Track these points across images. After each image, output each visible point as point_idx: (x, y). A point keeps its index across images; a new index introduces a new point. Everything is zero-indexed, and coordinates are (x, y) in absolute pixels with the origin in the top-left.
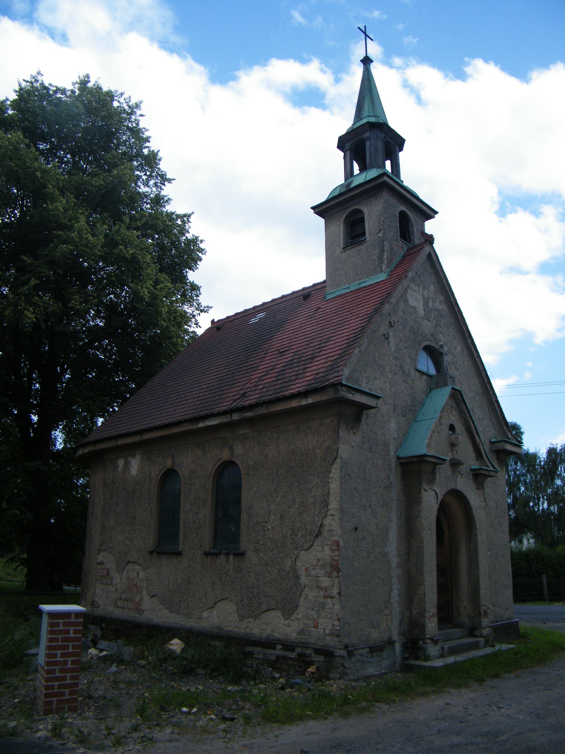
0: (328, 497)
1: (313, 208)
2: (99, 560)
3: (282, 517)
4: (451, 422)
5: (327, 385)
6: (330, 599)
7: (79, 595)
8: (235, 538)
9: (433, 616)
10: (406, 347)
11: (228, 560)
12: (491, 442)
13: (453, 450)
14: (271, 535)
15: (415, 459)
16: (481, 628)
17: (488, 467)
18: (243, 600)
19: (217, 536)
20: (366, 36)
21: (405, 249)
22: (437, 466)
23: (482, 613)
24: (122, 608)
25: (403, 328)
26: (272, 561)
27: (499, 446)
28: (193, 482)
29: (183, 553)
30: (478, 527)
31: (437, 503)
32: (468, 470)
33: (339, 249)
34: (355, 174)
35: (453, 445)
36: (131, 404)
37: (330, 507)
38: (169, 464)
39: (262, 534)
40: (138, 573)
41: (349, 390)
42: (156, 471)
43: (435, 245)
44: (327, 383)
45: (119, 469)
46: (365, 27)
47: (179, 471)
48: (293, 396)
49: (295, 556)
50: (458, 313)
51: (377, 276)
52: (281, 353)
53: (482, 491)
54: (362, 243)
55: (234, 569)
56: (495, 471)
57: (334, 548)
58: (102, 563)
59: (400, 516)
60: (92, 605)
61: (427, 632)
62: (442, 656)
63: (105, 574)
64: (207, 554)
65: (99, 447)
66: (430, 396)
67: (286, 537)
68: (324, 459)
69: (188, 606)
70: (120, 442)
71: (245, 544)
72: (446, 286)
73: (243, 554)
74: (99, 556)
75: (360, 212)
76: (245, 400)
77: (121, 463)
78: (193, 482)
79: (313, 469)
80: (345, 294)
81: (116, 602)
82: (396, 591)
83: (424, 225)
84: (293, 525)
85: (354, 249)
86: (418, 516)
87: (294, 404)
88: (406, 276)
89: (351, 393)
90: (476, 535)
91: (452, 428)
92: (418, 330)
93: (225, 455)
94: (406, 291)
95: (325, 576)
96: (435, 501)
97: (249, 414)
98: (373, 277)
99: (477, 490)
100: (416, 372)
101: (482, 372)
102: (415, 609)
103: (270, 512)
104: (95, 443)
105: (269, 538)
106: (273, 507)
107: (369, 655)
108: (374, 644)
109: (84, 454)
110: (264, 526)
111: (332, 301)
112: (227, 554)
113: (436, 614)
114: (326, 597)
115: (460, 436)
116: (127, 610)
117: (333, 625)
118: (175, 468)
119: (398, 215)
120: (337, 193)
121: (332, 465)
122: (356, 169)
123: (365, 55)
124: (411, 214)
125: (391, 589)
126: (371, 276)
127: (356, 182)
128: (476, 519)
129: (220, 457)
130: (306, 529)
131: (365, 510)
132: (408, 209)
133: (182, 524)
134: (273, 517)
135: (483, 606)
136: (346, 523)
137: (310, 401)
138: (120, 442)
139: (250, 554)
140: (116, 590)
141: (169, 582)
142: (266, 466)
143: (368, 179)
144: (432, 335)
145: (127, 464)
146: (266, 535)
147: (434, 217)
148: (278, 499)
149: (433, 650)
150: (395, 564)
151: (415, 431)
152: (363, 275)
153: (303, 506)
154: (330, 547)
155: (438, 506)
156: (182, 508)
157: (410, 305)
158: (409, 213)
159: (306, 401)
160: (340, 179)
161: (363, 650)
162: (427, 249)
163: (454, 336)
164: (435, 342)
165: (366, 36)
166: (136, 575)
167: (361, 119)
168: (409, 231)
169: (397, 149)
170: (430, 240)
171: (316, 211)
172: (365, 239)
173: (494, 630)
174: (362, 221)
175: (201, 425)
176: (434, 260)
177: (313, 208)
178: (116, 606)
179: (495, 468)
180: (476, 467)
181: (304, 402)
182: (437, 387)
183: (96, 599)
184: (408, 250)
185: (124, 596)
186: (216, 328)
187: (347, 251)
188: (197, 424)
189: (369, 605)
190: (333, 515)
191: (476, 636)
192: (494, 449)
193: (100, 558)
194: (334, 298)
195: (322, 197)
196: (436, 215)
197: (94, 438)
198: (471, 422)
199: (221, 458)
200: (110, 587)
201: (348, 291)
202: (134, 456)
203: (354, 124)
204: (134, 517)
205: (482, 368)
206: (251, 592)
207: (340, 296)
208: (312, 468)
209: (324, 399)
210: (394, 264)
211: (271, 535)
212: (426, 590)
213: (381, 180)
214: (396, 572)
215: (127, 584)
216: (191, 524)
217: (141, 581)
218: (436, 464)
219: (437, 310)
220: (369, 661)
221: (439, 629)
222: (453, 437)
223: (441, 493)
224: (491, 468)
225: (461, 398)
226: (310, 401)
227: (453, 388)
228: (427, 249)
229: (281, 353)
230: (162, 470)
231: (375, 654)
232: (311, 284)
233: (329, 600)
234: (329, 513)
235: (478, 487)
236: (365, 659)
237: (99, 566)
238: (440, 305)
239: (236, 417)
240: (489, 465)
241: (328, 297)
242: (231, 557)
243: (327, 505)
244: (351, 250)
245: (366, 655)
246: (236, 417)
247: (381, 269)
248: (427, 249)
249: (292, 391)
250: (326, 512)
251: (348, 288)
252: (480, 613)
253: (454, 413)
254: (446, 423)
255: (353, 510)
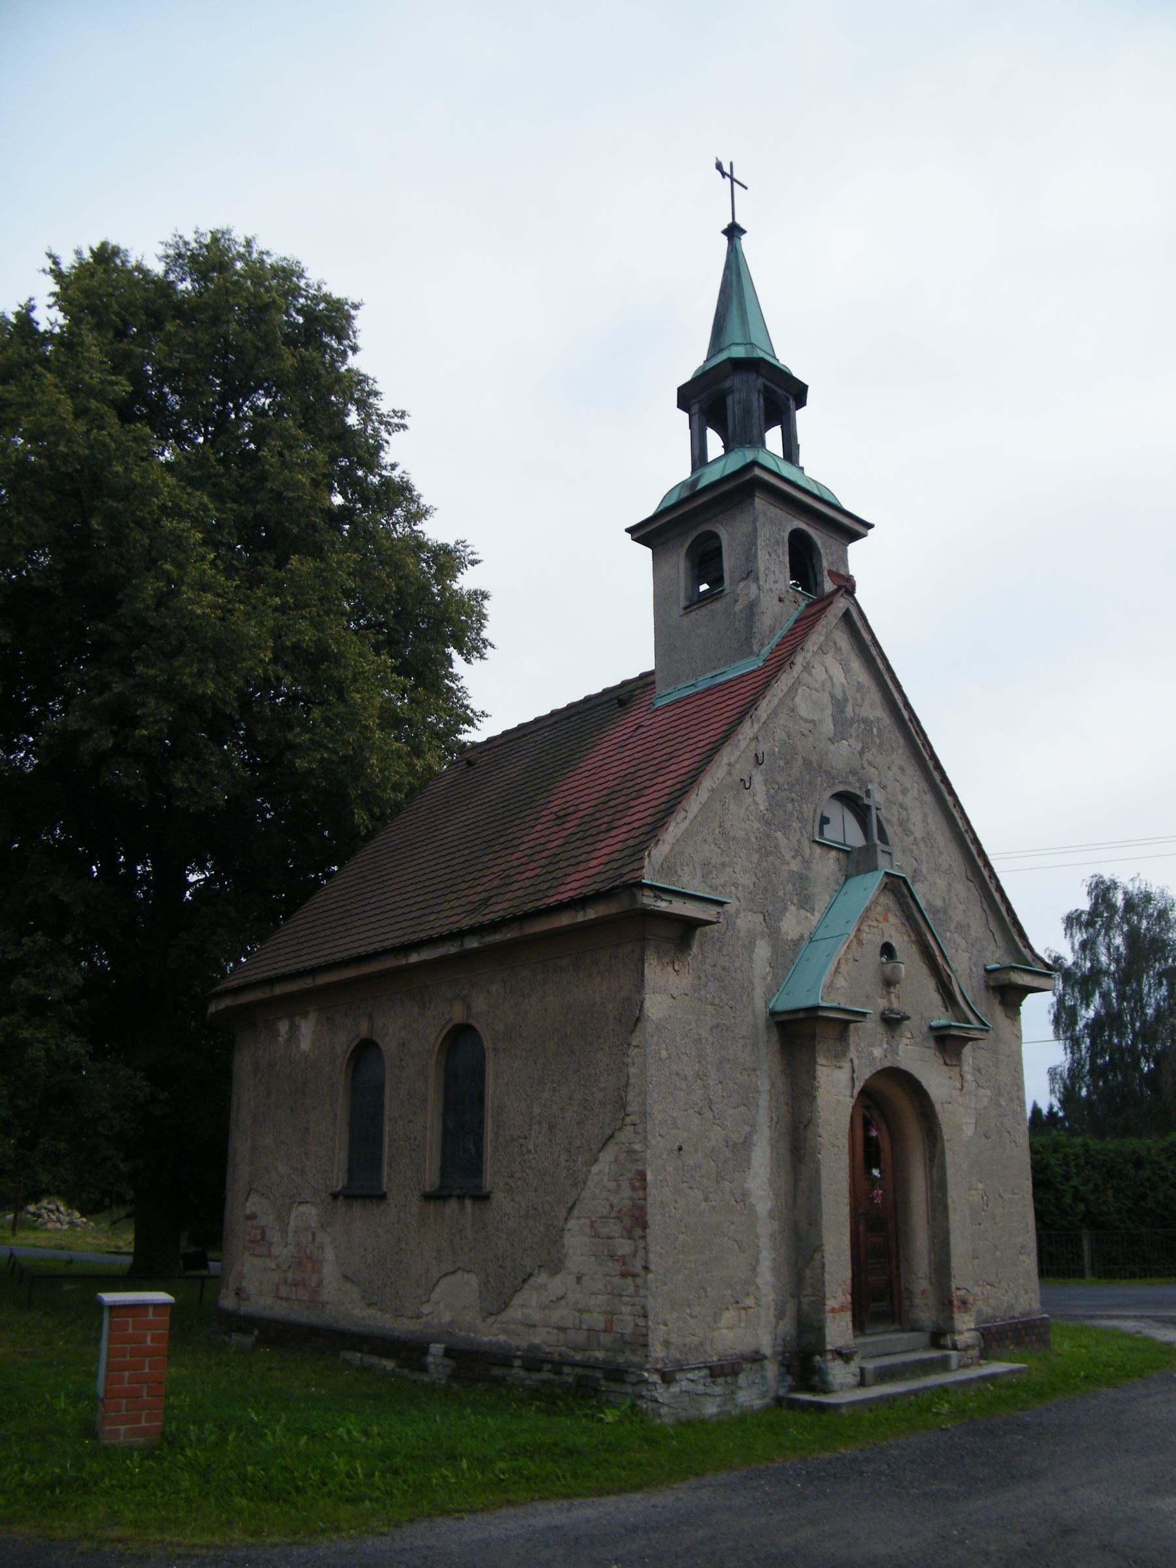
0: (626, 1092)
1: (628, 530)
2: (248, 1211)
3: (551, 1127)
4: (886, 940)
5: (617, 887)
6: (630, 1278)
7: (217, 1277)
8: (475, 1168)
9: (842, 1309)
10: (792, 800)
11: (463, 1208)
12: (986, 970)
13: (889, 993)
14: (533, 1162)
15: (801, 1015)
16: (953, 1333)
17: (969, 1022)
18: (489, 1282)
19: (448, 1165)
20: (733, 180)
21: (803, 604)
22: (852, 1026)
23: (956, 1302)
24: (288, 1299)
25: (787, 763)
26: (536, 1209)
27: (1004, 978)
28: (404, 1063)
29: (389, 1196)
30: (945, 1137)
31: (852, 1096)
32: (925, 1029)
33: (677, 610)
34: (709, 460)
35: (889, 983)
36: (303, 915)
37: (629, 1109)
38: (364, 1030)
39: (518, 1160)
40: (314, 1234)
41: (658, 893)
42: (342, 1043)
43: (856, 595)
44: (617, 883)
45: (281, 1039)
46: (731, 164)
47: (381, 1044)
48: (582, 902)
49: (573, 1200)
50: (910, 724)
51: (743, 662)
52: (561, 818)
53: (957, 1069)
54: (717, 599)
55: (473, 1225)
56: (981, 1030)
57: (637, 1184)
58: (253, 1217)
59: (777, 1123)
60: (237, 1294)
61: (828, 1339)
62: (862, 1384)
63: (259, 1237)
64: (428, 1197)
65: (244, 998)
66: (844, 891)
67: (558, 1165)
68: (620, 1021)
69: (397, 1293)
70: (278, 990)
71: (489, 1180)
72: (884, 672)
73: (486, 1197)
74: (248, 1204)
75: (715, 536)
76: (487, 910)
77: (283, 1027)
78: (404, 1063)
79: (602, 1040)
80: (688, 697)
81: (278, 1290)
82: (768, 1263)
83: (846, 552)
84: (570, 1143)
85: (703, 609)
86: (810, 1122)
87: (565, 920)
88: (792, 663)
89: (663, 900)
90: (943, 1153)
91: (887, 950)
92: (820, 766)
93: (458, 1014)
94: (792, 690)
95: (622, 1237)
96: (848, 1092)
97: (497, 937)
98: (738, 664)
99: (944, 1068)
100: (815, 847)
101: (966, 835)
102: (807, 1295)
103: (531, 1119)
104: (236, 991)
105: (530, 1168)
106: (536, 1110)
107: (709, 1380)
108: (719, 1360)
109: (217, 1012)
110: (522, 1145)
111: (739, 681)
112: (461, 1198)
113: (850, 1306)
114: (624, 1275)
115: (902, 966)
116: (296, 1303)
117: (636, 1325)
118: (375, 1038)
119: (786, 539)
120: (673, 500)
121: (633, 1032)
122: (715, 444)
123: (730, 221)
124: (816, 534)
125: (757, 1261)
126: (734, 662)
127: (711, 475)
128: (941, 1123)
129: (447, 1017)
130: (591, 1150)
131: (700, 1114)
132: (808, 525)
133: (386, 1141)
134: (536, 1127)
135: (958, 1289)
136: (660, 1138)
137: (591, 914)
138: (278, 990)
139: (499, 1196)
140: (278, 1267)
141: (365, 1250)
142: (524, 1034)
143: (728, 472)
144: (853, 772)
145: (294, 1029)
146: (525, 1161)
147: (865, 536)
148: (546, 1095)
149: (840, 1373)
150: (765, 1213)
151: (808, 960)
152: (719, 660)
153: (585, 1108)
154: (631, 1183)
155: (853, 1101)
156: (387, 1113)
157: (802, 718)
158: (812, 532)
159: (585, 914)
160: (682, 470)
161: (696, 1372)
162: (841, 605)
163: (902, 769)
164: (858, 785)
165: (733, 180)
166: (310, 1239)
167: (721, 350)
168: (813, 567)
169: (792, 403)
170: (847, 586)
171: (635, 537)
172: (723, 590)
173: (982, 1334)
174: (717, 553)
175: (414, 958)
176: (856, 625)
177: (628, 530)
178: (278, 1297)
179: (984, 1024)
180: (943, 1022)
181: (580, 917)
182: (858, 874)
183: (244, 1284)
184: (807, 606)
185: (290, 1275)
186: (615, 701)
187: (693, 613)
188: (406, 956)
189: (709, 1289)
190: (635, 1125)
191: (944, 1347)
192: (992, 983)
193: (250, 1208)
194: (667, 705)
195: (648, 509)
196: (870, 532)
197: (234, 983)
198: (929, 937)
199: (451, 1019)
200: (268, 1260)
201: (693, 690)
202: (305, 1015)
203: (708, 360)
204: (307, 1129)
205: (966, 827)
206: (501, 1267)
207: (677, 701)
208: (599, 1037)
209: (614, 911)
210: (777, 637)
211: (533, 1162)
212: (826, 1261)
213: (748, 477)
214: (766, 1229)
215: (295, 1255)
216: (402, 1142)
217: (318, 1248)
218: (848, 1022)
219: (865, 721)
220: (708, 1392)
221: (855, 1337)
222: (890, 966)
223: (865, 1074)
224: (976, 1024)
225: (906, 891)
226: (591, 914)
227: (886, 873)
228: (841, 604)
229: (561, 818)
230: (352, 1041)
231: (720, 1380)
232: (636, 675)
233: (629, 1280)
234: (628, 1120)
235: (948, 1061)
236: (700, 1388)
237: (249, 1223)
238: (873, 709)
239: (472, 943)
240: (971, 1017)
241: (660, 703)
242: (468, 1203)
243: (623, 1107)
244: (697, 611)
245: (702, 1381)
246: (472, 943)
247: (751, 647)
248: (841, 605)
249: (560, 897)
250: (623, 1119)
251: (693, 685)
252: (951, 1302)
253: (892, 919)
254: (873, 939)
255: (675, 1114)
